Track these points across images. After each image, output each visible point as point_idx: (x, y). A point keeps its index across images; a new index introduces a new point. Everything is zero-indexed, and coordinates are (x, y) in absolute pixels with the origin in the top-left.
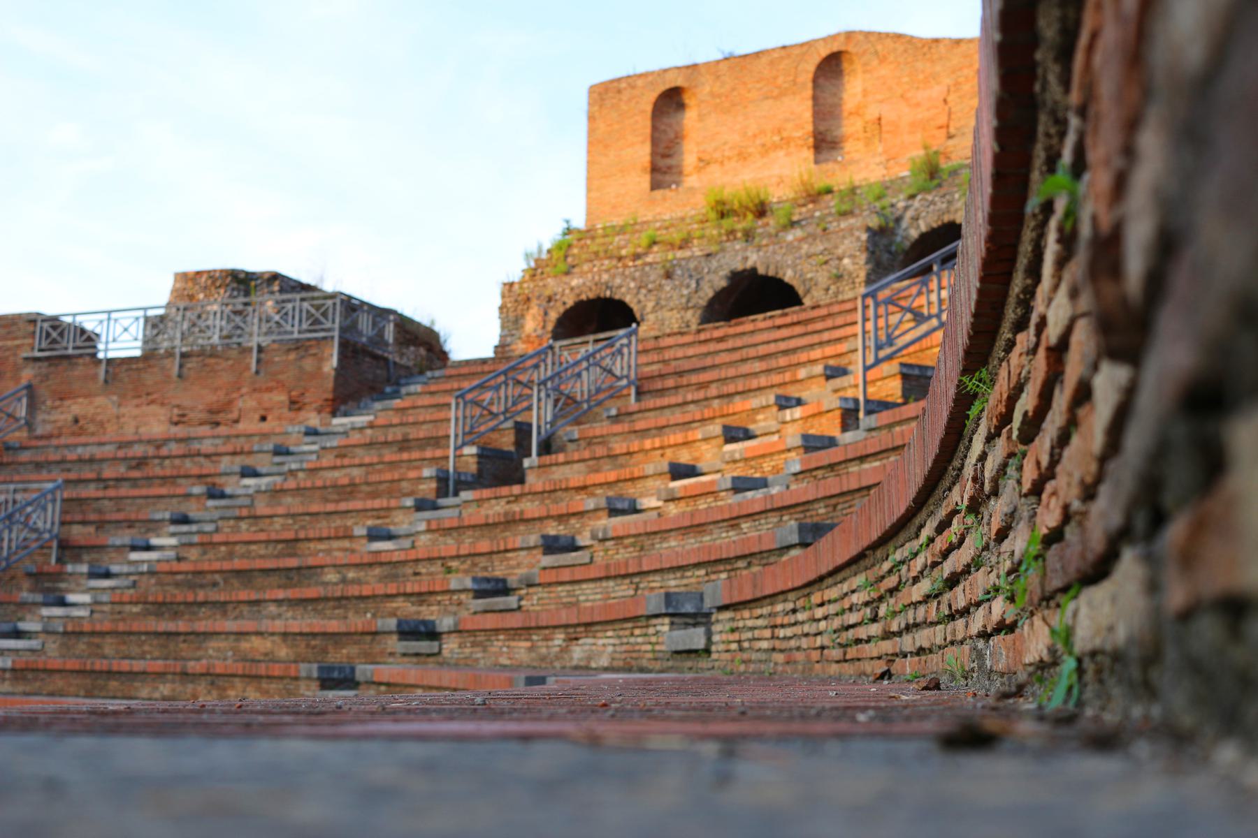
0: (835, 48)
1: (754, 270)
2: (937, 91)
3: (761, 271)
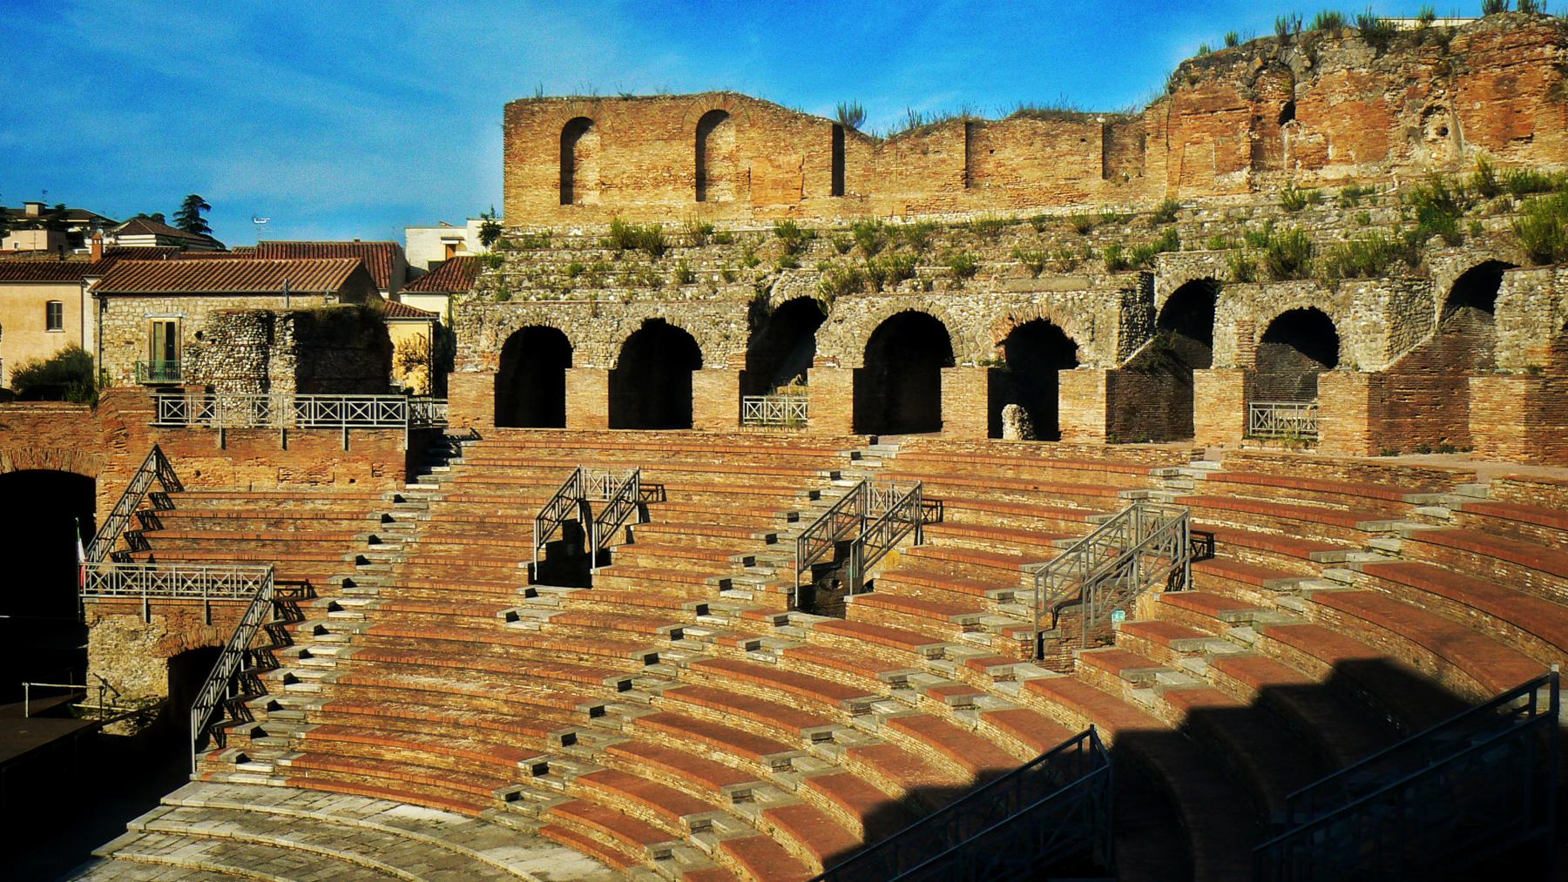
0: (717, 105)
1: (663, 320)
2: (794, 159)
3: (668, 321)
